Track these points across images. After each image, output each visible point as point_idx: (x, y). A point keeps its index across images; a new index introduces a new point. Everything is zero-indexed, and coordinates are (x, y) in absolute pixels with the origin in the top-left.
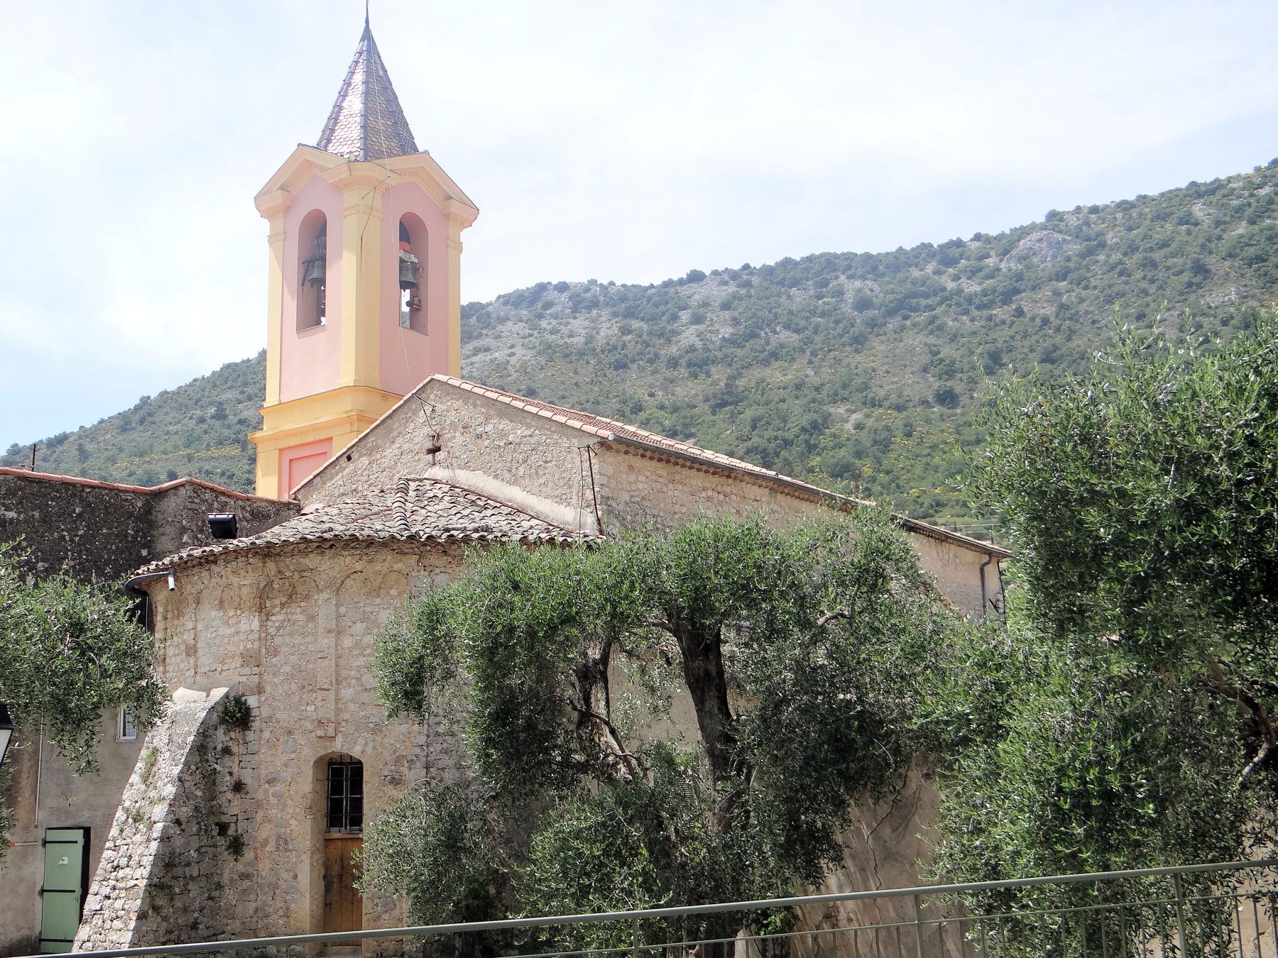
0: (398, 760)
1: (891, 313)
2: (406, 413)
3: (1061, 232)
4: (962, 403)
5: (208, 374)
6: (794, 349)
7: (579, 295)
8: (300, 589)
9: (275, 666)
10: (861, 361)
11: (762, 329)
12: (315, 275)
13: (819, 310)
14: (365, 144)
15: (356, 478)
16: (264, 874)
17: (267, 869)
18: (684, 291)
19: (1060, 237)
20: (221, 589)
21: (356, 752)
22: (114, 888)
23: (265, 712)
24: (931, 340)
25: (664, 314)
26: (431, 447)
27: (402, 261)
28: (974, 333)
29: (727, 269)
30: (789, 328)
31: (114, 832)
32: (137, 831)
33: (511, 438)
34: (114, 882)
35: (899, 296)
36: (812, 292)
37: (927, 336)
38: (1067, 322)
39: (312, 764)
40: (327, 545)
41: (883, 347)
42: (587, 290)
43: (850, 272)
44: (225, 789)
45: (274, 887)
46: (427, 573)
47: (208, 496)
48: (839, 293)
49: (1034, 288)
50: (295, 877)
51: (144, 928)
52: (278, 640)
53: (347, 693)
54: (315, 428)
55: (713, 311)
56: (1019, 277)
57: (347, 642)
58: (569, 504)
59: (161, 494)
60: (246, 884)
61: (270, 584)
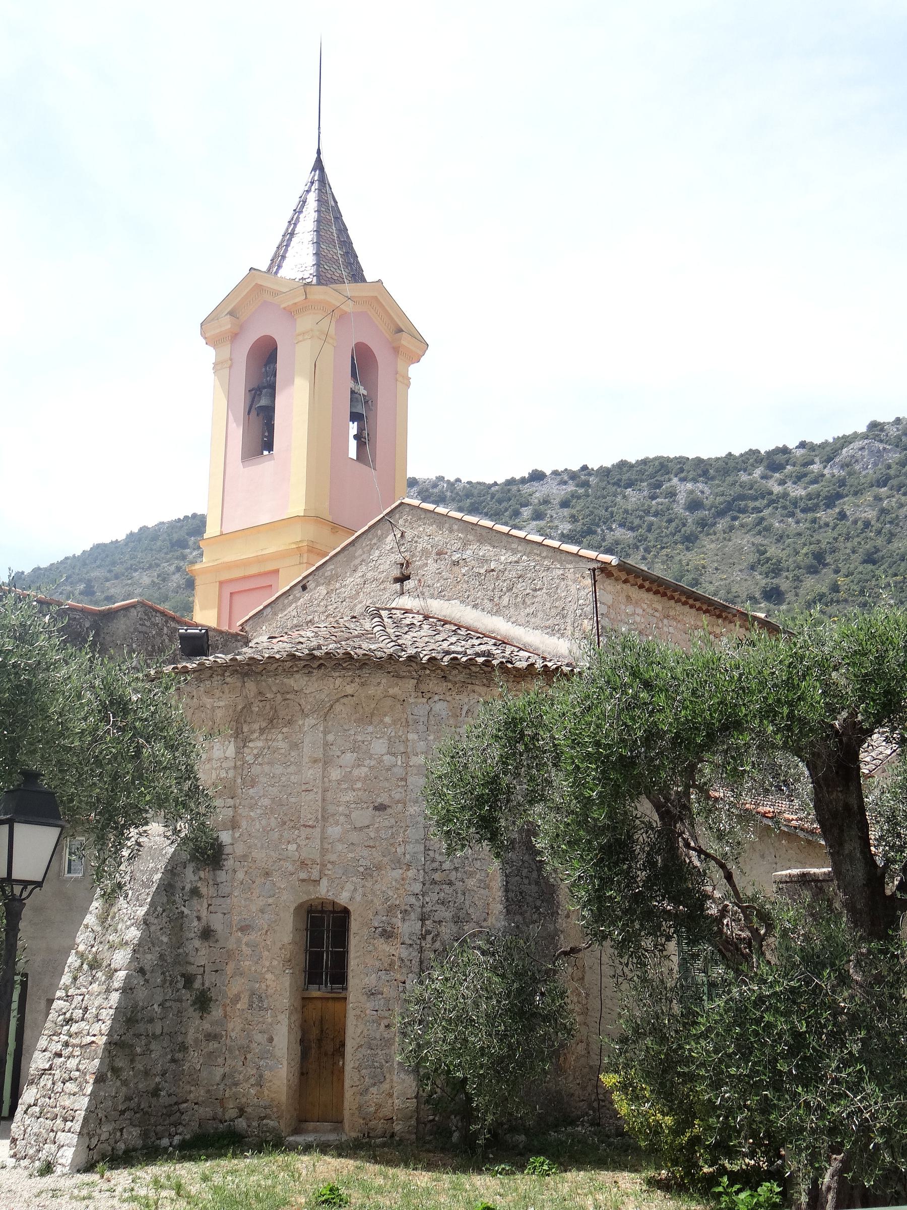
0: (391, 910)
1: (721, 514)
2: (371, 540)
3: (881, 441)
4: (787, 600)
5: (78, 553)
6: (629, 546)
7: (427, 490)
8: (282, 714)
9: (252, 798)
10: (693, 558)
11: (598, 526)
12: (263, 402)
13: (653, 510)
14: (317, 270)
15: (312, 609)
16: (233, 1035)
17: (238, 1029)
18: (526, 489)
19: (881, 446)
20: (192, 710)
21: (343, 899)
22: (66, 1044)
23: (240, 849)
24: (759, 540)
25: (506, 510)
26: (399, 575)
27: (353, 392)
28: (800, 534)
29: (566, 470)
30: (624, 526)
31: (66, 979)
32: (94, 979)
33: (493, 565)
34: (66, 1038)
35: (728, 499)
36: (646, 493)
37: (754, 536)
38: (888, 526)
39: (292, 910)
40: (316, 664)
41: (713, 546)
42: (435, 486)
43: (682, 475)
44: (193, 935)
45: (245, 1050)
46: (425, 700)
47: (158, 619)
48: (672, 494)
49: (856, 494)
50: (271, 1040)
51: (102, 1093)
52: (256, 769)
53: (334, 831)
54: (260, 560)
55: (552, 509)
56: (842, 483)
57: (335, 774)
58: (562, 635)
59: (109, 615)
60: (213, 1045)
61: (248, 706)
